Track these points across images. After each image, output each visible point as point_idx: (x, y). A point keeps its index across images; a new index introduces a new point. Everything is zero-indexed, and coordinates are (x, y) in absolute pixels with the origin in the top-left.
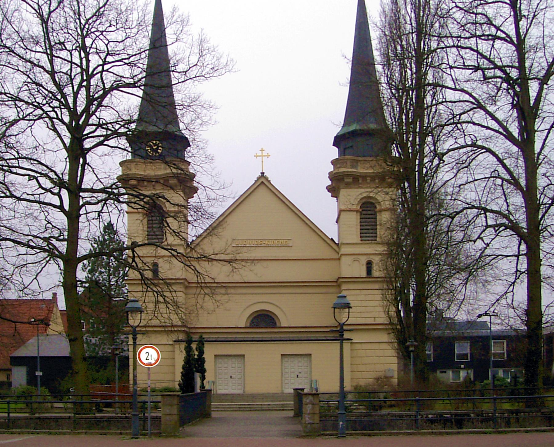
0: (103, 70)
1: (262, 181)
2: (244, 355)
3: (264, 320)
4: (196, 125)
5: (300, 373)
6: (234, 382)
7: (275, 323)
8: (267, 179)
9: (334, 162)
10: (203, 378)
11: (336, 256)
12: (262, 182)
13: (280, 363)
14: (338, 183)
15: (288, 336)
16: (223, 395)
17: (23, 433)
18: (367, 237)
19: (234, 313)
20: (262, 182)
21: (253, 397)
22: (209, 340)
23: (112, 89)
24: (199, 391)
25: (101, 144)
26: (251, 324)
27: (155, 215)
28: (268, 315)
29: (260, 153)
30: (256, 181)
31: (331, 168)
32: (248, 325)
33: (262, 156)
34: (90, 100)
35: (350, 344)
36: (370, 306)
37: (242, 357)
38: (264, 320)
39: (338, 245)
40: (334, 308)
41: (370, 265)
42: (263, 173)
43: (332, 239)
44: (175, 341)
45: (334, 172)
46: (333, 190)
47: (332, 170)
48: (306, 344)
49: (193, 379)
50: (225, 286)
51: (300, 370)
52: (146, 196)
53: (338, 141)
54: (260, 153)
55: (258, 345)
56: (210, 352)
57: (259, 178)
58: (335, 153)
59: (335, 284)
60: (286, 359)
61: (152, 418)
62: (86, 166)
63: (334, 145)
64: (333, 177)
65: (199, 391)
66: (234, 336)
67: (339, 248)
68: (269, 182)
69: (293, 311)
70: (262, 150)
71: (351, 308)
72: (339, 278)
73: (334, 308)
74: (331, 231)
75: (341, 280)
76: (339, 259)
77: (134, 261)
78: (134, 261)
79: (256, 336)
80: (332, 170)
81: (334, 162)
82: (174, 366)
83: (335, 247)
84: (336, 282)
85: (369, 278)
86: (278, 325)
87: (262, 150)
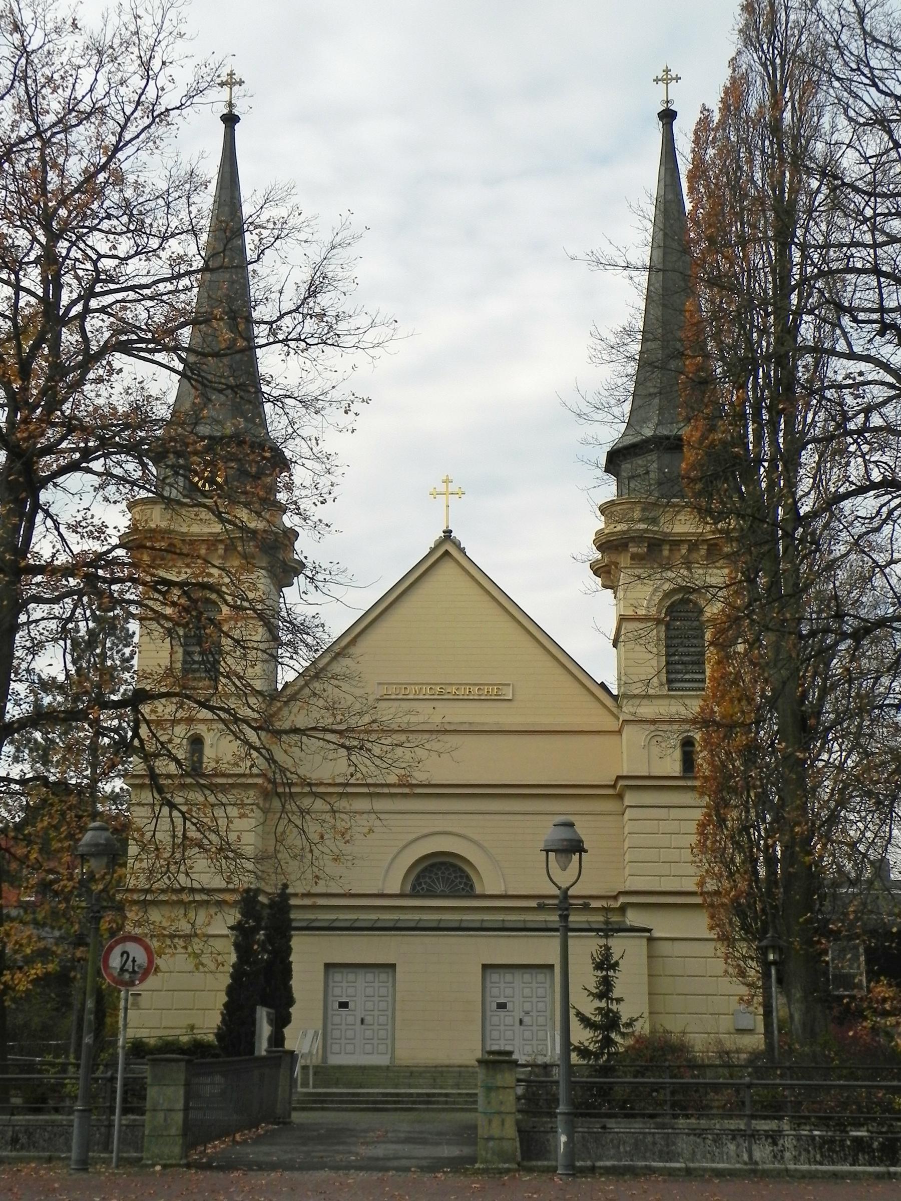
0: (87, 310)
1: (447, 550)
2: (393, 966)
3: (442, 874)
4: (620, 393)
5: (527, 1013)
6: (527, 1034)
7: (472, 887)
8: (457, 545)
9: (605, 509)
10: (281, 1020)
11: (614, 725)
12: (447, 553)
13: (321, 986)
14: (617, 554)
15: (334, 917)
16: (340, 1067)
18: (689, 681)
19: (376, 857)
20: (447, 553)
21: (412, 1073)
22: (357, 925)
23: (107, 349)
24: (264, 1053)
25: (73, 467)
26: (414, 887)
27: (196, 622)
29: (442, 488)
30: (433, 551)
31: (599, 523)
32: (408, 889)
34: (58, 370)
35: (645, 942)
36: (659, 848)
37: (390, 970)
38: (442, 874)
39: (615, 698)
40: (547, 851)
41: (687, 749)
42: (448, 532)
43: (603, 686)
45: (606, 531)
46: (605, 572)
47: (603, 526)
48: (546, 940)
49: (251, 1024)
50: (345, 790)
51: (527, 1006)
52: (169, 583)
53: (616, 460)
55: (427, 940)
56: (307, 958)
57: (439, 544)
58: (609, 490)
59: (610, 792)
60: (338, 977)
61: (72, 1121)
62: (40, 516)
63: (607, 470)
64: (604, 543)
65: (264, 1053)
66: (373, 916)
67: (620, 707)
68: (463, 551)
69: (509, 859)
71: (586, 851)
72: (619, 778)
73: (547, 851)
74: (604, 667)
75: (621, 783)
76: (619, 732)
77: (136, 734)
78: (136, 734)
79: (486, 917)
80: (603, 526)
81: (605, 509)
82: (650, 994)
83: (609, 702)
84: (614, 787)
85: (689, 778)
86: (478, 890)
87: (447, 481)
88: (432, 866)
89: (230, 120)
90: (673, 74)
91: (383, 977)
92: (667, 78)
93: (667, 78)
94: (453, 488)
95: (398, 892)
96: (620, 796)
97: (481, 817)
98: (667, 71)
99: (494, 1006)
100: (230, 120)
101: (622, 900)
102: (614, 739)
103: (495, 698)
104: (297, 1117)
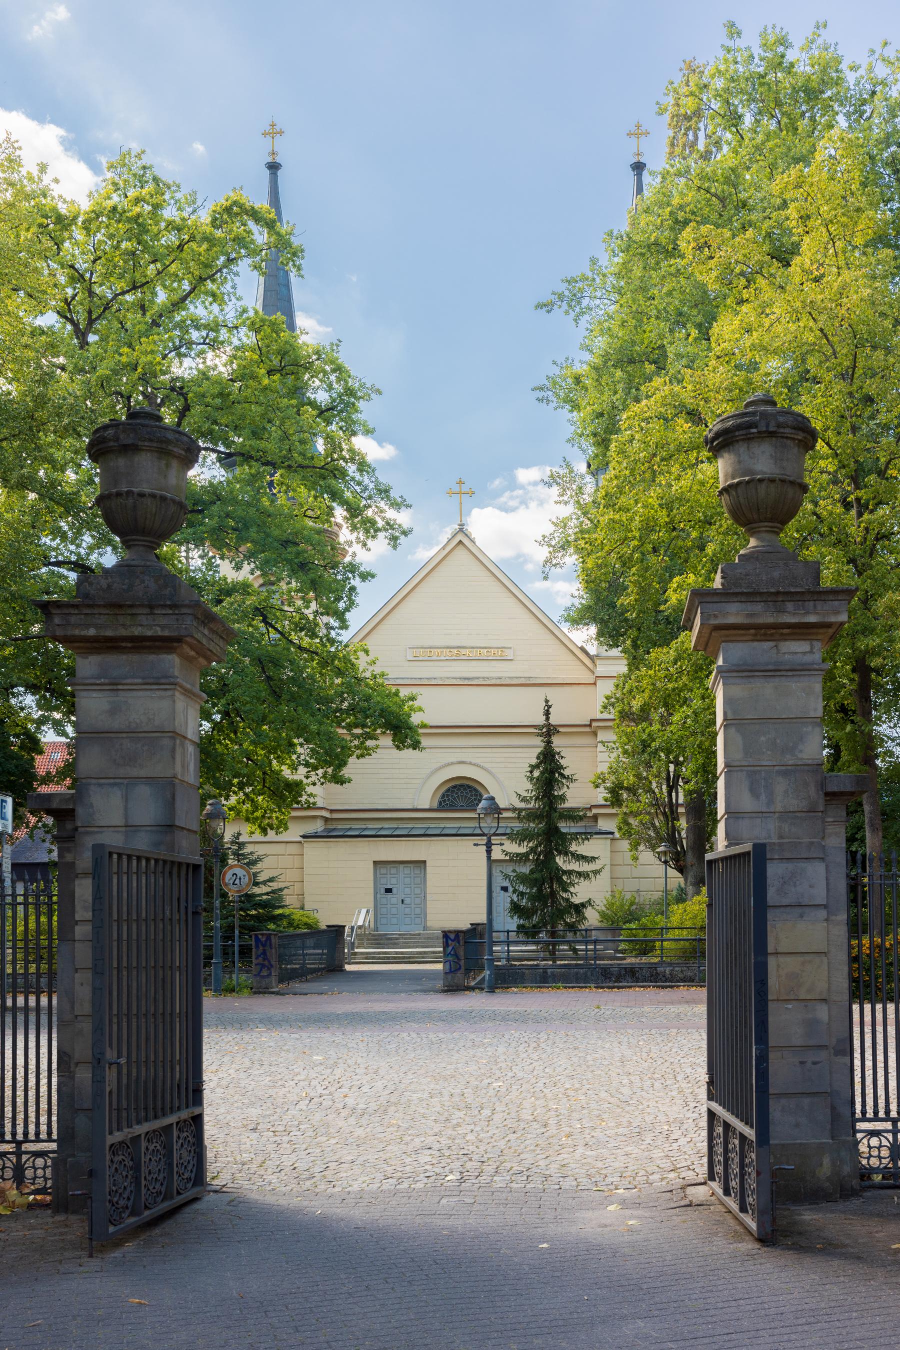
2: (425, 862)
12: (460, 542)
17: (373, 991)
20: (460, 542)
22: (460, 832)
26: (440, 803)
28: (469, 787)
29: (456, 488)
32: (435, 805)
33: (460, 493)
35: (609, 842)
44: (304, 837)
54: (456, 488)
55: (449, 843)
59: (587, 729)
60: (383, 871)
70: (460, 483)
72: (592, 720)
75: (594, 724)
83: (587, 661)
84: (590, 726)
87: (460, 483)
88: (462, 785)
89: (273, 167)
90: (278, 128)
91: (417, 871)
92: (273, 132)
93: (273, 132)
94: (465, 488)
95: (427, 807)
96: (595, 734)
97: (489, 750)
98: (638, 126)
99: (383, 891)
100: (273, 167)
101: (594, 811)
102: (592, 688)
103: (498, 656)
104: (348, 968)
